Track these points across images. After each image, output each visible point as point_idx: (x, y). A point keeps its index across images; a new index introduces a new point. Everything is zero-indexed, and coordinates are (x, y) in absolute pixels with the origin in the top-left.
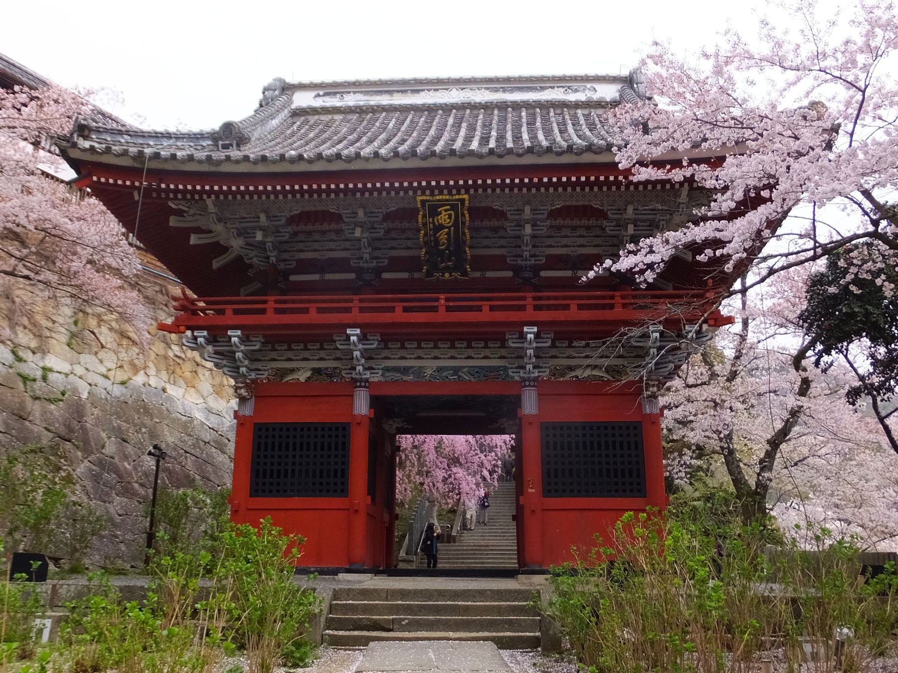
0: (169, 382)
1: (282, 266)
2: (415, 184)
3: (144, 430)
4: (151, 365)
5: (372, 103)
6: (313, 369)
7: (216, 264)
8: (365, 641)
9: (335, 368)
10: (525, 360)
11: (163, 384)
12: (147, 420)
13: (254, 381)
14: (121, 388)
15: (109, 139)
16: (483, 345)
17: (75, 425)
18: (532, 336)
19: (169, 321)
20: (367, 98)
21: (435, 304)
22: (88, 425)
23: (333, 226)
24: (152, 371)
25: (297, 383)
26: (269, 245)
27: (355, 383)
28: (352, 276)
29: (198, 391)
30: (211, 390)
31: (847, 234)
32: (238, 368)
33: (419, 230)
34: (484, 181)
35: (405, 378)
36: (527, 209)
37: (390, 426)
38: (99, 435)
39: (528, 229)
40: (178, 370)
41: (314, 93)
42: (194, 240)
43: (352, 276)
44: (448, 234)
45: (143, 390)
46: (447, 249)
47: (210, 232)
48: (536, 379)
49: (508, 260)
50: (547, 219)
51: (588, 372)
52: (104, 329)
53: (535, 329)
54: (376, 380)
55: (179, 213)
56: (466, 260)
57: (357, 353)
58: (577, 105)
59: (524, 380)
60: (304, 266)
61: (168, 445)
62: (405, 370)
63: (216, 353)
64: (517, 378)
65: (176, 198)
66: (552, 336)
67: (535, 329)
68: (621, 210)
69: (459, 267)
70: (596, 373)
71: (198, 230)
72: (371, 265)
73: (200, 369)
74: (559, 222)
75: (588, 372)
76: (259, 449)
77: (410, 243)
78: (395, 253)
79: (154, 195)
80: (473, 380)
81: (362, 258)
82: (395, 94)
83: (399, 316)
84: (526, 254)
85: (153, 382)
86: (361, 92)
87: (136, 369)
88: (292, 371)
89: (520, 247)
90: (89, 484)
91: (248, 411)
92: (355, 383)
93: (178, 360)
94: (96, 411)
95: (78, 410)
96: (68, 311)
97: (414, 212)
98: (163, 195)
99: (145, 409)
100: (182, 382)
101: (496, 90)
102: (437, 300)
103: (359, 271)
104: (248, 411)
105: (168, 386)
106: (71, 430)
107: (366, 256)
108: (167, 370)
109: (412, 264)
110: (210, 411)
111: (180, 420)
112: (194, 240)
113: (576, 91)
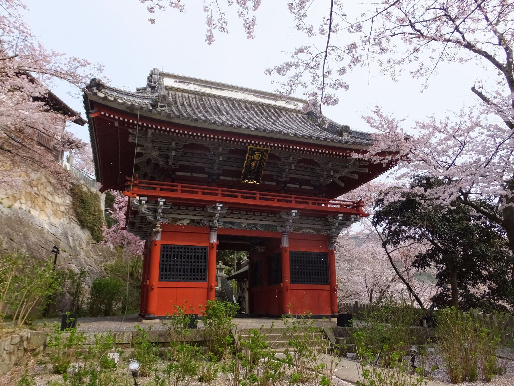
0: (32, 207)
2: (261, 143)
3: (21, 234)
4: (23, 197)
5: (202, 91)
6: (191, 220)
9: (201, 220)
11: (29, 209)
12: (21, 228)
14: (8, 209)
15: (126, 98)
16: (193, 209)
20: (199, 88)
24: (23, 201)
25: (183, 225)
27: (211, 228)
29: (46, 213)
30: (52, 213)
34: (289, 147)
35: (233, 227)
36: (174, 144)
41: (174, 80)
44: (256, 164)
45: (19, 211)
49: (274, 177)
51: (308, 230)
54: (220, 227)
59: (283, 232)
60: (182, 168)
61: (33, 243)
62: (233, 224)
64: (280, 231)
70: (310, 231)
73: (47, 201)
75: (308, 230)
76: (163, 257)
80: (262, 230)
82: (213, 89)
83: (239, 200)
85: (24, 207)
87: (15, 199)
93: (36, 196)
99: (21, 223)
100: (38, 208)
101: (258, 97)
102: (256, 194)
105: (31, 209)
107: (215, 168)
108: (31, 201)
110: (51, 224)
111: (37, 229)
113: (290, 104)
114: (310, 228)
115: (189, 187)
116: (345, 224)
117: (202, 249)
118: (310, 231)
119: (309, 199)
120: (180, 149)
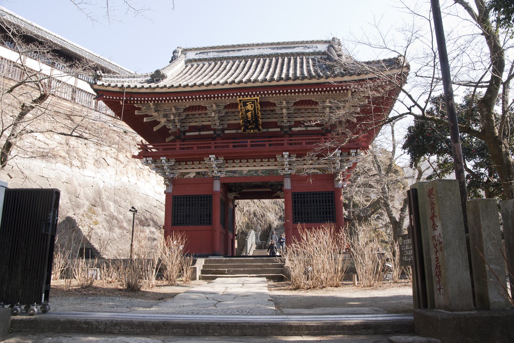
1: (182, 129)
5: (220, 56)
6: (197, 172)
7: (155, 129)
8: (215, 278)
10: (285, 166)
12: (129, 197)
13: (172, 178)
17: (98, 199)
18: (339, 154)
19: (136, 154)
20: (218, 54)
21: (246, 144)
22: (104, 200)
23: (203, 112)
25: (190, 178)
26: (177, 121)
28: (212, 132)
31: (401, 113)
32: (165, 173)
33: (239, 112)
35: (235, 175)
36: (284, 102)
37: (231, 196)
38: (108, 203)
39: (284, 111)
40: (141, 175)
42: (145, 120)
43: (212, 132)
44: (252, 114)
46: (252, 120)
47: (152, 116)
48: (290, 174)
49: (278, 123)
50: (293, 106)
52: (109, 157)
53: (288, 153)
54: (222, 176)
55: (139, 109)
56: (259, 124)
57: (214, 165)
58: (309, 54)
62: (235, 172)
63: (156, 167)
64: (282, 174)
65: (137, 103)
66: (295, 156)
67: (288, 153)
68: (324, 102)
69: (257, 127)
70: (315, 171)
71: (147, 116)
72: (220, 128)
74: (299, 107)
75: (312, 171)
77: (236, 118)
78: (230, 122)
79: (129, 102)
81: (216, 125)
84: (285, 121)
86: (215, 52)
88: (188, 173)
89: (282, 118)
90: (105, 224)
91: (170, 191)
92: (214, 178)
94: (107, 193)
95: (99, 194)
96: (93, 150)
97: (236, 105)
98: (132, 102)
102: (247, 142)
103: (215, 130)
104: (170, 191)
105: (138, 182)
106: (96, 202)
107: (285, 121)
109: (237, 127)
112: (145, 120)
113: (309, 48)
114: (315, 168)
115: (239, 142)
116: (349, 160)
117: (319, 194)
118: (315, 171)
119: (302, 140)
120: (291, 107)
